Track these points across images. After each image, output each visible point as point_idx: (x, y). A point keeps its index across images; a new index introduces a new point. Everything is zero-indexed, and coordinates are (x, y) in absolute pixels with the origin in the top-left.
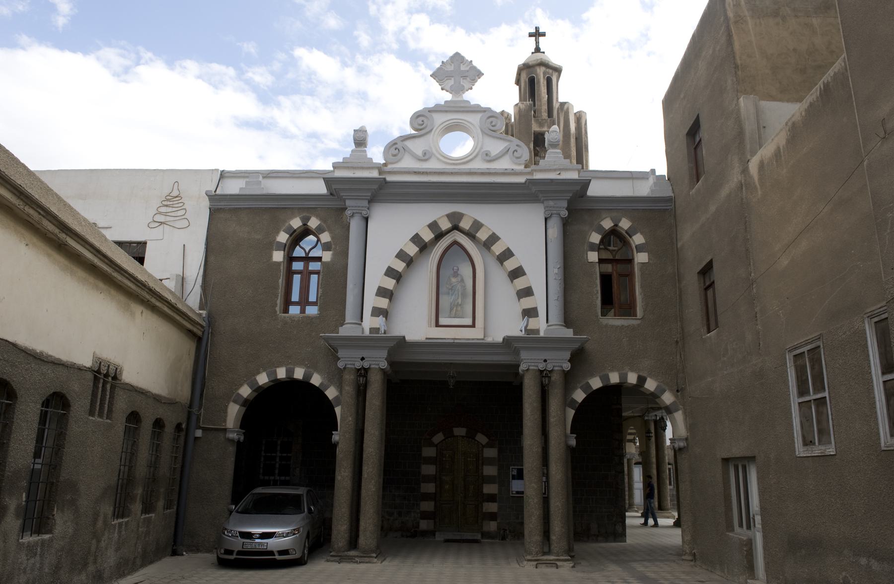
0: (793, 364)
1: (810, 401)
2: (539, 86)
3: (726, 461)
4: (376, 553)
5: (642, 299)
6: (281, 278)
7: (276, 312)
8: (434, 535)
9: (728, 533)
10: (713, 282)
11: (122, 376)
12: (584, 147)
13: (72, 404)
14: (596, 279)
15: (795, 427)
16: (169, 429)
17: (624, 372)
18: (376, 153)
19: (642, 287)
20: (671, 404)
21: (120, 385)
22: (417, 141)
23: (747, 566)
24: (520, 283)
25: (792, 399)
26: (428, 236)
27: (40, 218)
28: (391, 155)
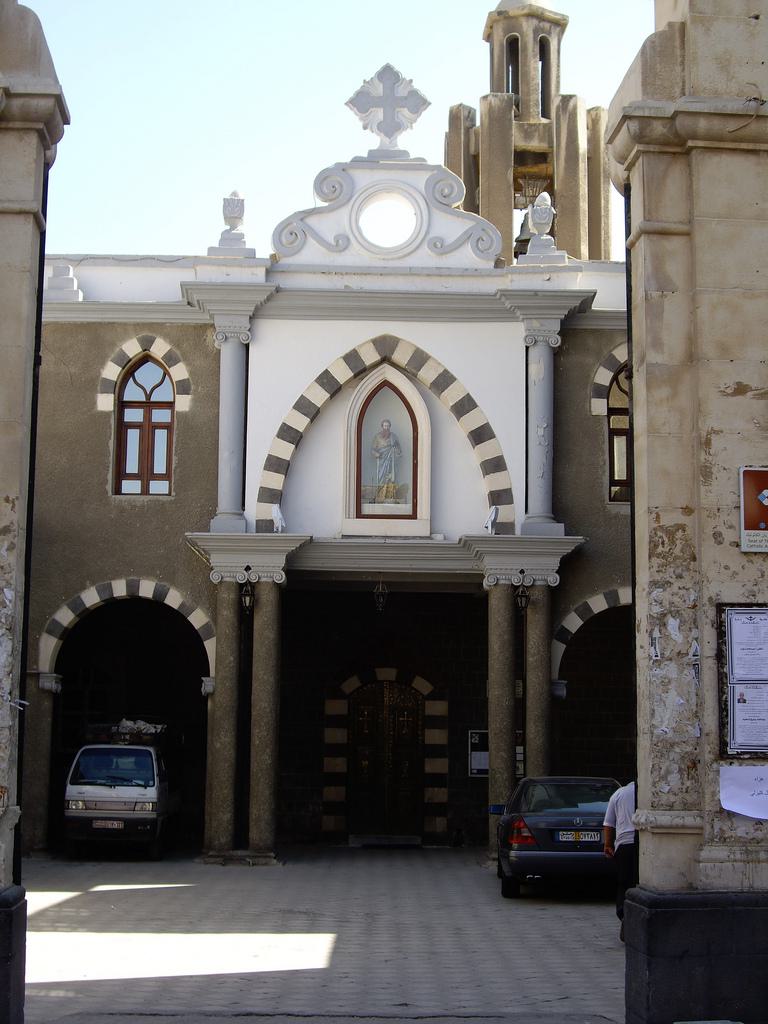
12: (602, 174)
14: (603, 442)
18: (260, 241)
24: (488, 450)
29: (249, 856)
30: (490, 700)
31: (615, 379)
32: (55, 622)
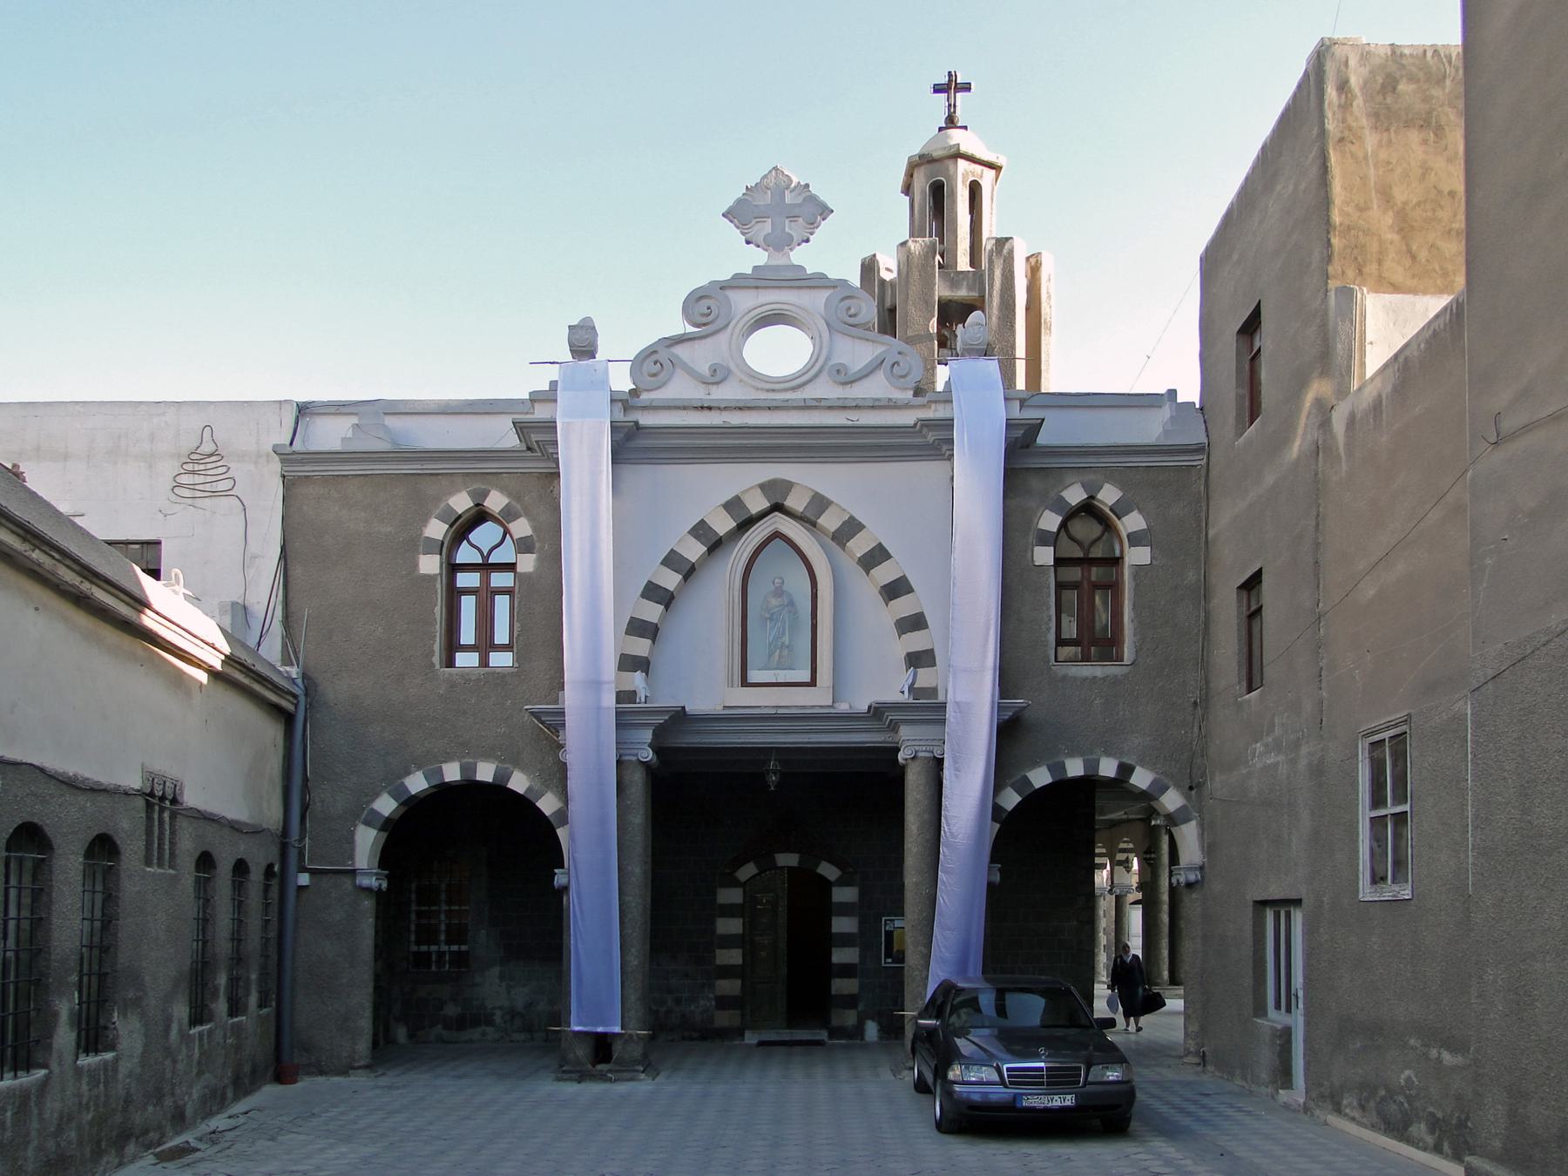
0: (1367, 756)
1: (1387, 815)
2: (954, 202)
3: (1262, 904)
4: (643, 1065)
5: (1135, 630)
6: (439, 603)
7: (433, 665)
8: (742, 1035)
9: (1255, 1019)
10: (1261, 607)
11: (182, 797)
13: (122, 850)
15: (1361, 856)
16: (256, 875)
17: (1094, 757)
19: (1135, 607)
20: (1178, 810)
21: (183, 812)
22: (697, 345)
23: (1280, 1068)
25: (1360, 812)
26: (723, 524)
27: (55, 565)
28: (646, 374)
29: (610, 1071)
30: (906, 888)
31: (1063, 525)
32: (374, 812)
